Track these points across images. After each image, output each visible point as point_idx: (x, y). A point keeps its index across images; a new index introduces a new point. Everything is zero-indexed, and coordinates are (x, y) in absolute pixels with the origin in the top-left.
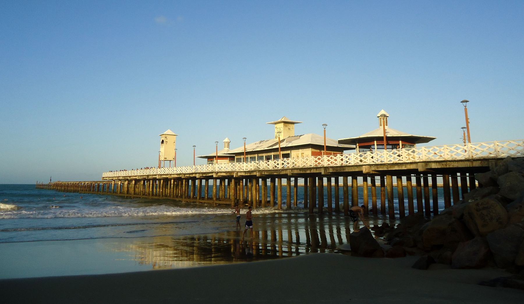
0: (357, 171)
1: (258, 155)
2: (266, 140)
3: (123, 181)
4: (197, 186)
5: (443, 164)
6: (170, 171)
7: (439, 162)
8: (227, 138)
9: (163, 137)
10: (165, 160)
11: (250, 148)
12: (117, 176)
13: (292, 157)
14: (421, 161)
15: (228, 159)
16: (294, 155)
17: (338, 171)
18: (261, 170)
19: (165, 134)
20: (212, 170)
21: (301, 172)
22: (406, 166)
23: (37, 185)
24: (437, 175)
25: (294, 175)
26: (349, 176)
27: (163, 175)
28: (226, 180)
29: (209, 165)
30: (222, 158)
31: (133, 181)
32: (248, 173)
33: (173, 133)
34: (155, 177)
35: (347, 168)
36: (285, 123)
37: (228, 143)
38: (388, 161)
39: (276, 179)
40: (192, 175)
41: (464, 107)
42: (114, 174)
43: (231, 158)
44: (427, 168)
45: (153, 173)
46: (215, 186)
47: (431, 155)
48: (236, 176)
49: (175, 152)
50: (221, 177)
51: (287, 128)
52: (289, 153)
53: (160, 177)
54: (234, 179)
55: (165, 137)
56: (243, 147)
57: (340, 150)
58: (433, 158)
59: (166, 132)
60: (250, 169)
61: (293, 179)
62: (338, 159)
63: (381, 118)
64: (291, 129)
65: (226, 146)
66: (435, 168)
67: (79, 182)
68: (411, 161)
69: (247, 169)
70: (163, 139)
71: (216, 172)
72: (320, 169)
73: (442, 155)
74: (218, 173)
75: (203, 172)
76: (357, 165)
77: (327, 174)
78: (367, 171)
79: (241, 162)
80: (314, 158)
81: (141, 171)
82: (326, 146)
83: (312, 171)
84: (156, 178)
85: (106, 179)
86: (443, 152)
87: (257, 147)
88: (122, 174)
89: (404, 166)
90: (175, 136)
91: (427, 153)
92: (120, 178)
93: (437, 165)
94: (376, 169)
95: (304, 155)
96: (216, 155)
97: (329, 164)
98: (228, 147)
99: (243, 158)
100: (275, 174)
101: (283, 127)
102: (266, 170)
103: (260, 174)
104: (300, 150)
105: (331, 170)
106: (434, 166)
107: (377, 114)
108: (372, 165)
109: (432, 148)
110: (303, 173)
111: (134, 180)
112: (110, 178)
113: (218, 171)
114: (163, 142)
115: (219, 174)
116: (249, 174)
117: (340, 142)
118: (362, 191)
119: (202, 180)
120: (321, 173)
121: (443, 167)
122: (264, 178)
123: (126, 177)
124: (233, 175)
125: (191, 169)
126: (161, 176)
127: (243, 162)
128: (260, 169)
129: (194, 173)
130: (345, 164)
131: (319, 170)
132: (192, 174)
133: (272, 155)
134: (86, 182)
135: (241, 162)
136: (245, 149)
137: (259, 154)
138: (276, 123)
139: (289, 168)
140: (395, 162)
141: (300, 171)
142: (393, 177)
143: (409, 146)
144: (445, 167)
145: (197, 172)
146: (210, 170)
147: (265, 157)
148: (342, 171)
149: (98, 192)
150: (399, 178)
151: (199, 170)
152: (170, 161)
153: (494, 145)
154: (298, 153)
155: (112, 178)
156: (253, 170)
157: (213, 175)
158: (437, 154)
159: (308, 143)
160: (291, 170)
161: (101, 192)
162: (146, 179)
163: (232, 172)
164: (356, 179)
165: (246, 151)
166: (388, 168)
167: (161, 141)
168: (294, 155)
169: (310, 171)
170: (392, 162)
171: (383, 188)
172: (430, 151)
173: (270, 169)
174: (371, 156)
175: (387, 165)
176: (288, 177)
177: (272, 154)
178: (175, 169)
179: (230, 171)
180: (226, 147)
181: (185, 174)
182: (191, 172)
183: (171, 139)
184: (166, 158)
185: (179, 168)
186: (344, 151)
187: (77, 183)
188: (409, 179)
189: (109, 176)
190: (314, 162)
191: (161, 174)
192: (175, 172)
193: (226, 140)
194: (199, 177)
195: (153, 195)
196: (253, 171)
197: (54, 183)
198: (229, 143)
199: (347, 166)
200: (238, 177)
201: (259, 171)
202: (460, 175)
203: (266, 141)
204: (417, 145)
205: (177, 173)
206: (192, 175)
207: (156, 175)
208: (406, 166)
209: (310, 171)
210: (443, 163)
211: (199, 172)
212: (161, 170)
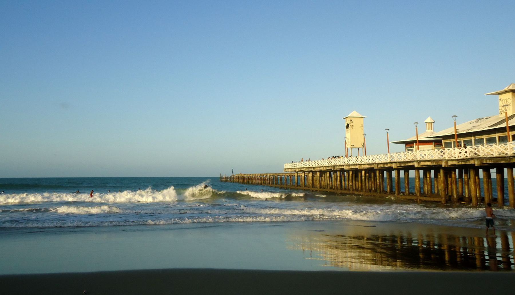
1: (475, 138)
2: (486, 118)
9: (348, 120)
11: (463, 129)
12: (300, 167)
15: (432, 144)
18: (481, 158)
19: (350, 117)
20: (413, 159)
27: (351, 165)
29: (408, 153)
31: (318, 172)
33: (360, 115)
34: (342, 167)
37: (431, 124)
39: (384, 171)
40: (387, 165)
41: (416, 127)
43: (437, 142)
46: (417, 178)
49: (345, 141)
53: (348, 167)
55: (350, 120)
56: (454, 127)
65: (429, 127)
67: (261, 174)
69: (460, 157)
71: (417, 161)
74: (420, 161)
88: (305, 165)
90: (362, 118)
92: (303, 170)
96: (416, 140)
98: (431, 129)
99: (454, 142)
100: (502, 162)
111: (318, 171)
112: (292, 170)
113: (421, 160)
114: (348, 126)
115: (422, 163)
116: (463, 163)
123: (310, 168)
124: (441, 164)
125: (386, 158)
126: (349, 167)
128: (479, 156)
129: (389, 163)
132: (387, 163)
133: (496, 137)
134: (268, 174)
135: (451, 147)
137: (476, 137)
138: (500, 94)
145: (393, 161)
151: (395, 158)
152: (359, 148)
155: (294, 170)
157: (414, 165)
163: (439, 160)
164: (408, 172)
165: (457, 133)
167: (346, 125)
177: (497, 135)
179: (436, 159)
181: (378, 164)
182: (385, 162)
184: (354, 146)
187: (258, 175)
189: (291, 168)
191: (348, 164)
192: (366, 162)
193: (429, 120)
194: (396, 167)
195: (341, 189)
196: (469, 159)
198: (432, 124)
206: (387, 165)
207: (343, 166)
211: (395, 161)
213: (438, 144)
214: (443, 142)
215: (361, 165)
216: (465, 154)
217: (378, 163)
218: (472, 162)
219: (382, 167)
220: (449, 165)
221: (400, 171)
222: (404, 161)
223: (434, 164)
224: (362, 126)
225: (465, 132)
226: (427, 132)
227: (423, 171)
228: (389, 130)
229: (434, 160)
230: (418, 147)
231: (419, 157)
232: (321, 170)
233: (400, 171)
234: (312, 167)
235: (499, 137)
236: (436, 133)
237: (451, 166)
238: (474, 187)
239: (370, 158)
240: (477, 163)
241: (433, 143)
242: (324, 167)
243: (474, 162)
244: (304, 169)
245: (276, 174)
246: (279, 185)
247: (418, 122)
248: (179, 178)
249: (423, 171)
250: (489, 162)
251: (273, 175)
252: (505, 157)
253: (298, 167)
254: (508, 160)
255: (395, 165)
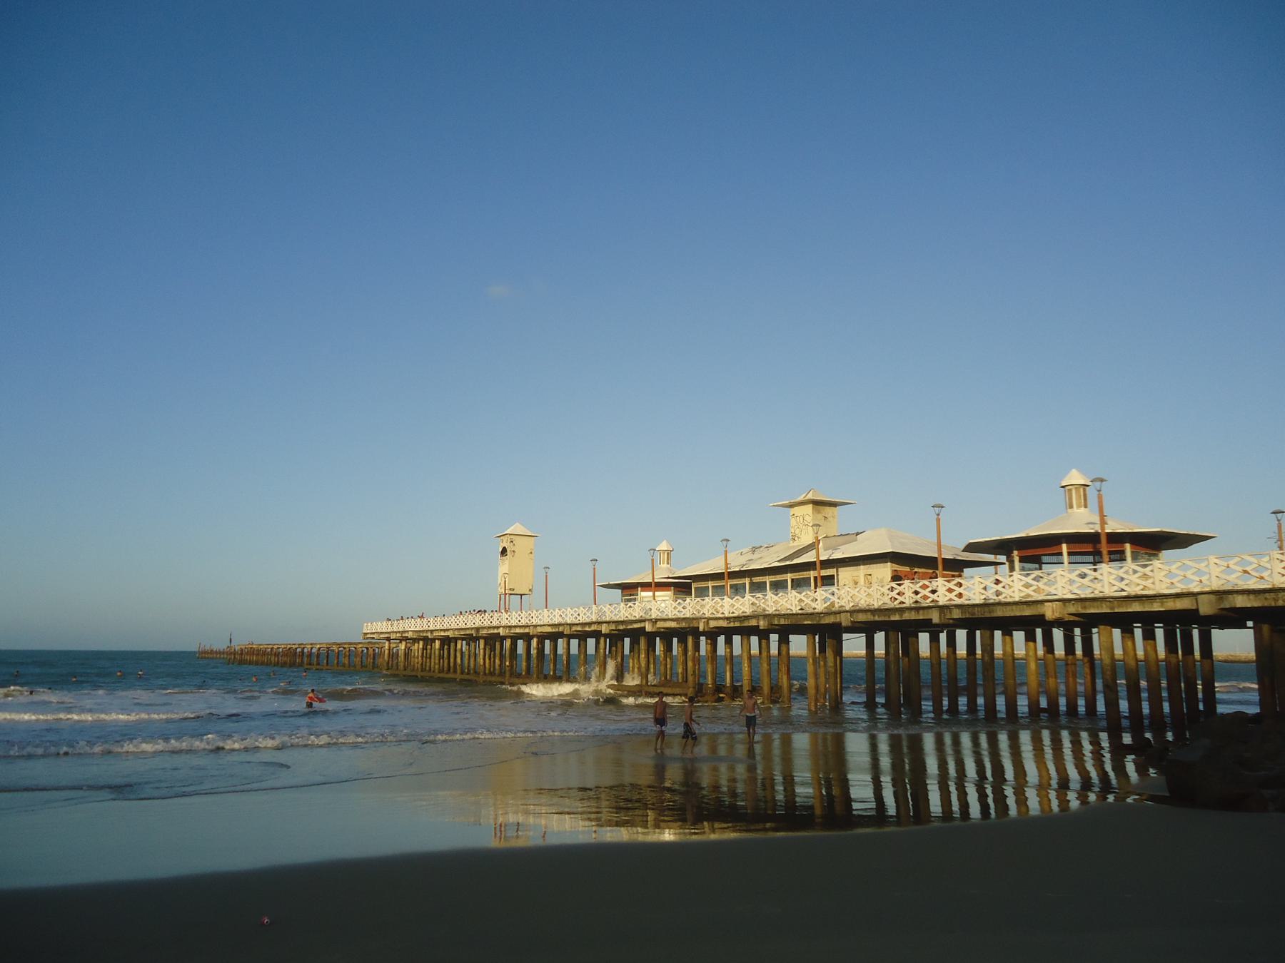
0: (1027, 614)
1: (751, 580)
2: (766, 546)
3: (395, 643)
4: (562, 655)
5: (1268, 597)
6: (532, 617)
7: (1255, 593)
8: (665, 541)
9: (504, 541)
10: (511, 594)
11: (738, 562)
12: (401, 630)
13: (841, 583)
14: (1207, 589)
15: (670, 590)
16: (846, 580)
17: (977, 616)
18: (770, 615)
19: (510, 534)
20: (641, 616)
21: (877, 618)
22: (1162, 603)
23: (199, 651)
24: (1156, 625)
25: (857, 625)
26: (1081, 630)
27: (515, 627)
28: (625, 639)
30: (664, 588)
31: (437, 641)
32: (734, 622)
33: (528, 531)
34: (496, 631)
35: (999, 608)
36: (816, 503)
37: (668, 554)
38: (1113, 590)
39: (546, 641)
40: (590, 627)
41: (936, 517)
42: (392, 625)
43: (682, 587)
44: (1222, 606)
45: (491, 622)
46: (643, 652)
47: (1234, 576)
48: (704, 629)
49: (545, 574)
50: (663, 632)
51: (820, 516)
52: (834, 575)
53: (507, 631)
54: (645, 636)
55: (509, 540)
57: (955, 567)
58: (1240, 582)
59: (512, 528)
60: (741, 611)
61: (774, 638)
62: (906, 591)
63: (1070, 490)
64: (830, 519)
65: (664, 559)
66: (1244, 606)
67: (299, 645)
68: (1178, 591)
69: (733, 613)
70: (505, 545)
71: (651, 620)
72: (926, 611)
73: (1265, 574)
74: (657, 621)
75: (620, 619)
76: (1030, 602)
77: (947, 621)
78: (1057, 615)
79: (708, 596)
80: (797, 594)
81: (460, 620)
82: (1108, 534)
83: (907, 616)
84: (499, 633)
85: (373, 638)
86: (1205, 573)
87: (750, 560)
88: (413, 626)
89: (1157, 602)
90: (533, 538)
91: (1221, 572)
92: (406, 635)
93: (1249, 599)
94: (1080, 609)
95: (874, 580)
97: (951, 600)
98: (668, 563)
99: (816, 578)
100: (806, 623)
101: (811, 514)
102: (784, 615)
103: (767, 622)
104: (862, 566)
105: (956, 614)
106: (1240, 602)
107: (1061, 480)
108: (1070, 600)
109: (1237, 559)
110: (880, 619)
111: (438, 639)
112: (382, 636)
113: (658, 617)
114: (504, 551)
115: (660, 624)
116: (737, 624)
117: (971, 548)
118: (1026, 666)
119: (594, 639)
120: (931, 620)
121: (1266, 604)
122: (1067, 626)
123: (423, 631)
124: (696, 626)
125: (588, 614)
126: (510, 630)
127: (816, 588)
128: (767, 613)
129: (594, 623)
130: (993, 598)
131: (923, 614)
132: (590, 624)
133: (787, 580)
134: (316, 644)
135: (708, 596)
136: (727, 564)
137: (753, 579)
138: (791, 506)
139: (844, 609)
140: (1133, 594)
141: (874, 616)
142: (571, 640)
143: (1146, 556)
144: (1273, 604)
145: (604, 619)
146: (637, 615)
147: (770, 585)
148: (987, 615)
149: (373, 669)
150: (1128, 632)
151: (607, 615)
152: (521, 595)
153: (1270, 559)
154: (855, 573)
155: (386, 636)
156: (748, 614)
157: (645, 627)
158: (1249, 574)
159: (1015, 534)
160: (849, 614)
161: (323, 666)
162: (471, 638)
163: (693, 619)
164: (1011, 635)
165: (729, 570)
166: (1112, 608)
167: (501, 550)
168: (845, 578)
169: (901, 616)
170: (1124, 594)
171: (1070, 657)
172: (1230, 566)
173: (794, 612)
174: (983, 586)
175: (1111, 600)
176: (764, 635)
177: (789, 577)
178: (505, 615)
179: (688, 616)
180: (663, 564)
181: (571, 625)
182: (588, 620)
183: (522, 545)
184: (514, 590)
185: (557, 610)
186: (965, 570)
188: (1149, 636)
189: (379, 631)
190: (912, 595)
191: (509, 624)
192: (546, 621)
193: (664, 546)
194: (608, 632)
195: (485, 674)
196: (748, 616)
197: (239, 647)
198: (669, 553)
199: (999, 604)
200: (709, 630)
201: (765, 616)
202: (1252, 626)
203: (767, 547)
204: (1165, 554)
205: (551, 622)
206: (590, 627)
207: (498, 628)
208: (1162, 603)
209: (901, 616)
210: (1267, 594)
211: (608, 619)
212: (509, 616)
213: (679, 589)
214: (694, 586)
215: (535, 626)
216: (983, 591)
217: (573, 622)
218: (753, 623)
219: (579, 631)
220: (712, 626)
221: (734, 636)
222: (626, 619)
223: (683, 625)
224: (531, 553)
225: (738, 570)
226: (661, 568)
227: (629, 639)
228: (942, 507)
229: (684, 619)
230: (654, 594)
231: (655, 612)
232: (448, 636)
233: (734, 636)
234: (427, 631)
235: (792, 580)
236: (679, 572)
237: (714, 630)
238: (748, 667)
239: (533, 615)
240: (762, 624)
241: (672, 588)
242: (456, 629)
243: (758, 623)
244: (410, 633)
245: (334, 644)
246: (323, 666)
247: (1105, 478)
248: (176, 652)
249: (629, 639)
250: (783, 623)
251: (328, 646)
252: (812, 614)
253: (395, 630)
254: (817, 618)
255: (606, 628)
